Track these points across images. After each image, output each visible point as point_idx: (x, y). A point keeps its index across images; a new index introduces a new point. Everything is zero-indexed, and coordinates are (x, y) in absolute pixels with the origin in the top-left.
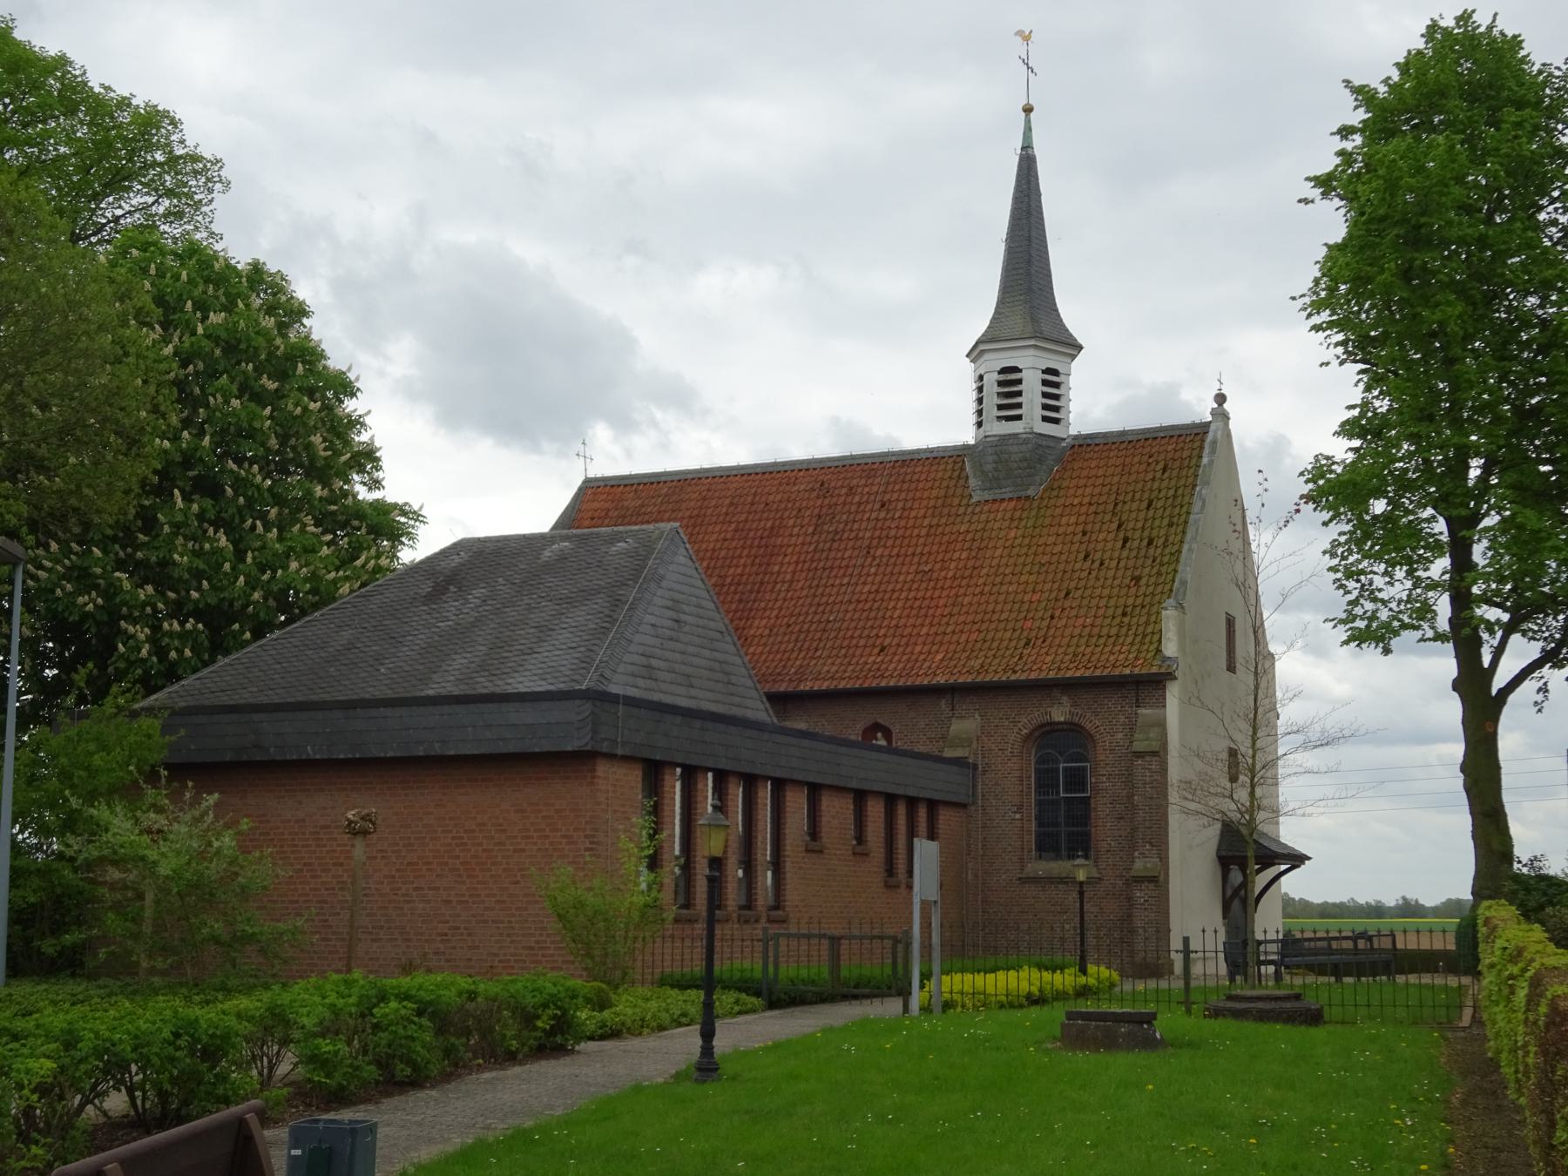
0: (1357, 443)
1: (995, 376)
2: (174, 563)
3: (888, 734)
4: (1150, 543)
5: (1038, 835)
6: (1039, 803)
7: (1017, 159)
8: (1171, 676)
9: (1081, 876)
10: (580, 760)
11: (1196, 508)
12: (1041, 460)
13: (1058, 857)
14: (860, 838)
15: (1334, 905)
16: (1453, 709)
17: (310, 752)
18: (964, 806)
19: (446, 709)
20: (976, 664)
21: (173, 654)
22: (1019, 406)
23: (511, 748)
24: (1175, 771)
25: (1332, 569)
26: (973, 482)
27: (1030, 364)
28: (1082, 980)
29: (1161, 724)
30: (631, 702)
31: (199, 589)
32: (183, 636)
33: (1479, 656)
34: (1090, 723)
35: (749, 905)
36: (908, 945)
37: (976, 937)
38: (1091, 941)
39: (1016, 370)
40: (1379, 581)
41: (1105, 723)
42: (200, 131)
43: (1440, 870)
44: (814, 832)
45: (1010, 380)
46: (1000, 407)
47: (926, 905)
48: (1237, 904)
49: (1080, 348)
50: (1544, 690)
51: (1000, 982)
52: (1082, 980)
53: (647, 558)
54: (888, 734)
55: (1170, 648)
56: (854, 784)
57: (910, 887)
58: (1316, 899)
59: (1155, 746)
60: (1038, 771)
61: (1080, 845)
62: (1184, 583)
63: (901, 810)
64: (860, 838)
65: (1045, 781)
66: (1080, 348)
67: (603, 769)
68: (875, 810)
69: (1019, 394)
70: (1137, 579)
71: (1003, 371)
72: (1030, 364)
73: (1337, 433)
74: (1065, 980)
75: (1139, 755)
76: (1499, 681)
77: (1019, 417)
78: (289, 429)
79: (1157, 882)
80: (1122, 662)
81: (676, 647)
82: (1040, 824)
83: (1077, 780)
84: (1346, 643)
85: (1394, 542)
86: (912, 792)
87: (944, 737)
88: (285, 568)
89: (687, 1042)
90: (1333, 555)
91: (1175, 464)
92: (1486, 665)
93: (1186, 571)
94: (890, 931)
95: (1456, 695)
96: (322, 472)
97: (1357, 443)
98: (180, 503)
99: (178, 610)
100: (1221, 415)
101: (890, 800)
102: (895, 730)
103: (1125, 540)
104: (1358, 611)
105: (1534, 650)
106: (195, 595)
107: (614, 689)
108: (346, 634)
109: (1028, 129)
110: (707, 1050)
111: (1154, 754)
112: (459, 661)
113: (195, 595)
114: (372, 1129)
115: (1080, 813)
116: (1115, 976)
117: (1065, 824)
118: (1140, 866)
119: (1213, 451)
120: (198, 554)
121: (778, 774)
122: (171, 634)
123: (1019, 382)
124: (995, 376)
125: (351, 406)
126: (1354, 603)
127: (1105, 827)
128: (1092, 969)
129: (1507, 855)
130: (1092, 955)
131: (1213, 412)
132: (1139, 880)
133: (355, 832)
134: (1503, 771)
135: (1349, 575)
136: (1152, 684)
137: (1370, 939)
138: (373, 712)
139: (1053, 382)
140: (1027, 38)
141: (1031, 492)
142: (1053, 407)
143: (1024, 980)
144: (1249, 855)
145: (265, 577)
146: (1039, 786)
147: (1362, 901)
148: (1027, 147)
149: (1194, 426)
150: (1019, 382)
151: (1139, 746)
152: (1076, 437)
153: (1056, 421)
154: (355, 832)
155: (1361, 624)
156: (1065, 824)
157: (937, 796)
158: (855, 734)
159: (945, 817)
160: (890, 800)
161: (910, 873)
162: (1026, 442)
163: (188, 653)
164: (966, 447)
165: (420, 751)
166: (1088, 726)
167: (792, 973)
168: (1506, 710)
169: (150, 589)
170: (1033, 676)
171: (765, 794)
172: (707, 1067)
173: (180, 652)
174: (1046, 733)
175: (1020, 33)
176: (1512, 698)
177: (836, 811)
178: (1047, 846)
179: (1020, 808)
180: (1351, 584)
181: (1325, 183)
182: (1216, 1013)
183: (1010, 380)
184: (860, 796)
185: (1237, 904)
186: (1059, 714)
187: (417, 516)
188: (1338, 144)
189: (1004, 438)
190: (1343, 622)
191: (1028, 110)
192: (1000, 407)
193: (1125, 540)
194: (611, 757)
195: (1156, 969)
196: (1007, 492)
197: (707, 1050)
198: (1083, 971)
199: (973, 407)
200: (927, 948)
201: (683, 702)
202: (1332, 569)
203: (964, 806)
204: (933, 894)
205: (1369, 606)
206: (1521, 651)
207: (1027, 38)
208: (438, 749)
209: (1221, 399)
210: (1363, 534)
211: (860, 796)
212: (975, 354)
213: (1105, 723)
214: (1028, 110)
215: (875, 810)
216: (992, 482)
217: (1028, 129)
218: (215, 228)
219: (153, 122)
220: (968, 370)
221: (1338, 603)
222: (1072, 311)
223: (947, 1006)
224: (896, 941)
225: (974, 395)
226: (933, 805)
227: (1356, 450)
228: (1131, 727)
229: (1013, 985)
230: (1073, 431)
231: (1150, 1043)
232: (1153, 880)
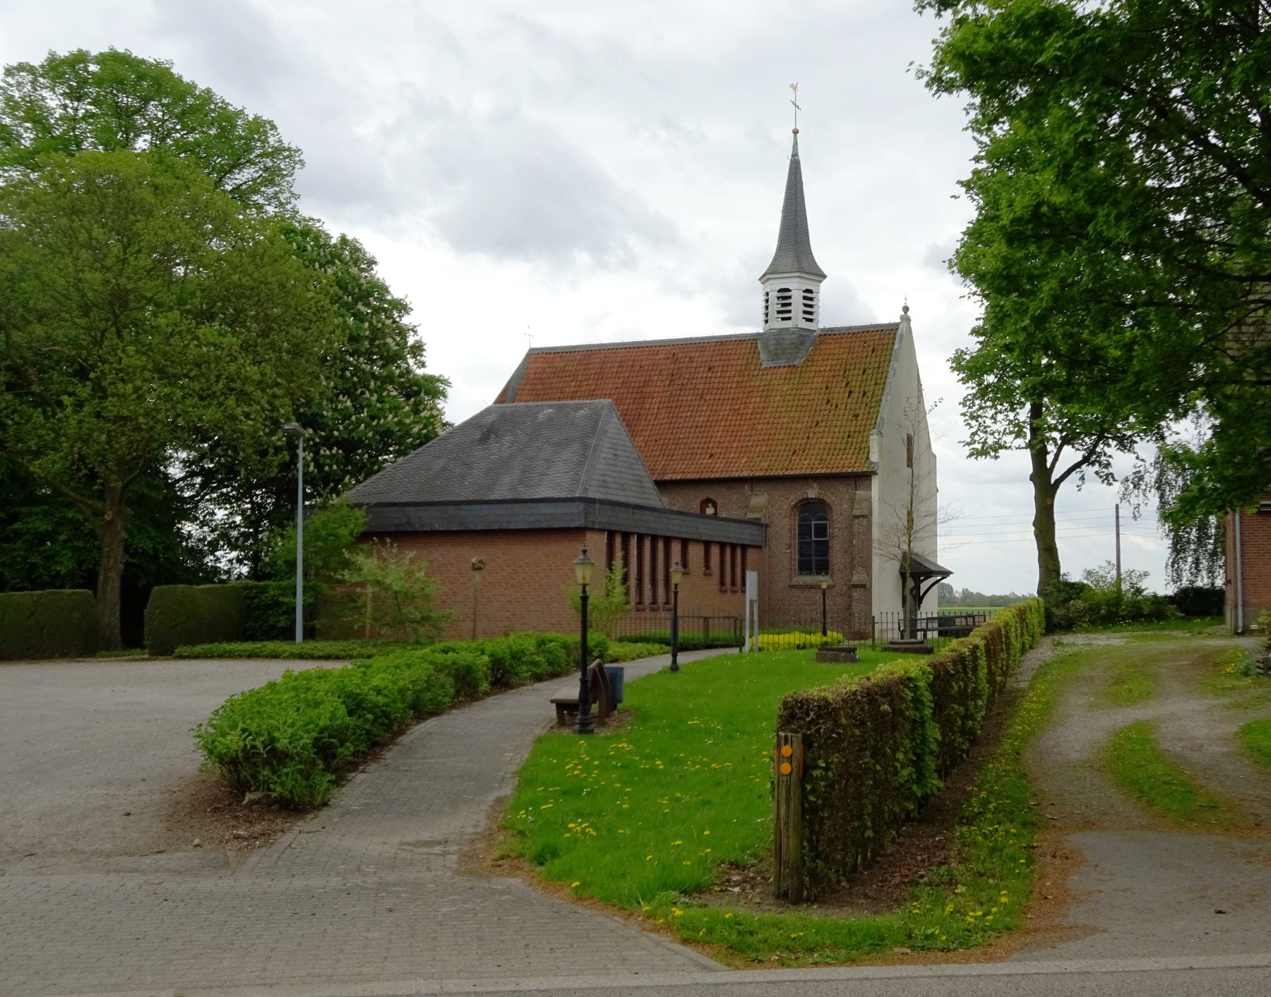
0: (982, 339)
1: (777, 294)
2: (323, 416)
3: (715, 505)
4: (865, 394)
5: (800, 562)
6: (800, 543)
7: (788, 162)
8: (875, 473)
9: (824, 586)
10: (579, 531)
11: (890, 375)
12: (802, 344)
13: (811, 574)
14: (707, 566)
15: (1000, 597)
16: (1029, 491)
17: (437, 527)
18: (759, 547)
19: (509, 506)
20: (765, 465)
21: (327, 468)
22: (790, 311)
23: (543, 525)
24: (876, 533)
25: (964, 414)
26: (762, 356)
27: (796, 286)
28: (825, 639)
29: (869, 500)
30: (602, 502)
31: (338, 430)
32: (332, 456)
33: (1045, 461)
34: (829, 498)
35: (654, 602)
36: (743, 621)
37: (771, 619)
38: (829, 620)
39: (788, 290)
40: (989, 422)
41: (837, 498)
42: (287, 134)
43: (1023, 580)
44: (685, 565)
45: (784, 295)
46: (779, 312)
47: (752, 602)
48: (914, 598)
49: (825, 277)
50: (1082, 478)
51: (784, 639)
52: (825, 639)
53: (597, 421)
54: (715, 505)
55: (874, 457)
56: (705, 538)
57: (744, 592)
58: (988, 593)
59: (865, 512)
60: (800, 526)
61: (823, 567)
62: (883, 419)
63: (728, 551)
64: (707, 566)
65: (804, 531)
66: (825, 277)
67: (589, 535)
68: (715, 551)
69: (790, 304)
70: (856, 416)
71: (781, 291)
72: (796, 286)
73: (972, 333)
74: (816, 638)
75: (857, 517)
76: (1055, 476)
77: (789, 319)
78: (376, 334)
79: (865, 587)
80: (847, 464)
81: (610, 465)
82: (801, 555)
83: (821, 531)
84: (970, 456)
85: (1003, 395)
86: (734, 541)
87: (747, 507)
88: (386, 418)
89: (667, 660)
90: (965, 406)
91: (880, 347)
92: (1048, 465)
93: (884, 412)
94: (734, 614)
95: (1031, 484)
96: (391, 358)
97: (982, 339)
98: (324, 383)
99: (328, 442)
100: (906, 319)
101: (722, 545)
102: (719, 502)
103: (850, 392)
104: (977, 438)
105: (1079, 456)
106: (336, 433)
107: (591, 495)
108: (440, 463)
109: (796, 144)
110: (674, 661)
111: (865, 516)
112: (507, 479)
113: (336, 433)
114: (622, 669)
115: (824, 548)
116: (840, 636)
117: (814, 557)
118: (856, 579)
119: (901, 341)
120: (335, 410)
121: (668, 534)
122: (325, 456)
123: (790, 297)
124: (777, 294)
125: (406, 320)
126: (974, 434)
127: (837, 557)
128: (829, 633)
129: (1057, 570)
130: (828, 626)
131: (902, 317)
132: (855, 586)
133: (476, 568)
134: (1057, 527)
135: (972, 418)
136: (863, 478)
137: (974, 617)
138: (472, 507)
139: (809, 295)
140: (794, 88)
141: (796, 363)
142: (809, 314)
143: (796, 637)
144: (918, 573)
145: (375, 423)
146: (800, 534)
147: (1019, 594)
148: (795, 155)
149: (890, 325)
150: (790, 297)
151: (857, 512)
152: (822, 330)
153: (811, 320)
154: (476, 568)
155: (979, 446)
156: (814, 557)
157: (747, 543)
158: (695, 507)
159: (751, 554)
160: (722, 545)
161: (744, 584)
162: (793, 333)
163: (335, 467)
164: (758, 334)
165: (496, 527)
166: (828, 500)
167: (686, 635)
168: (1059, 491)
169: (311, 431)
170: (797, 472)
171: (676, 548)
172: (675, 668)
173: (331, 467)
174: (805, 506)
175: (792, 86)
176: (1062, 485)
177: (696, 552)
178: (804, 567)
179: (789, 547)
180: (973, 423)
181: (967, 185)
182: (886, 649)
183: (784, 295)
184: (707, 544)
185: (914, 598)
186: (813, 492)
187: (446, 382)
188: (974, 166)
189: (780, 330)
190: (968, 444)
191: (796, 132)
192: (779, 312)
193: (850, 392)
194: (593, 529)
195: (861, 636)
196: (783, 363)
197: (674, 661)
198: (825, 634)
199: (763, 310)
200: (752, 622)
201: (622, 499)
202: (964, 414)
203: (759, 547)
204: (755, 597)
205: (982, 435)
206: (1071, 455)
207: (794, 88)
208: (505, 526)
209: (906, 309)
210: (983, 392)
211: (707, 544)
212: (764, 279)
213: (837, 498)
214: (796, 132)
215: (715, 551)
216: (774, 356)
217: (796, 144)
218: (294, 190)
219: (260, 128)
220: (760, 289)
221: (966, 434)
222: (821, 252)
223: (760, 649)
224: (736, 619)
225: (764, 304)
226: (744, 547)
227: (981, 343)
228: (852, 501)
229: (792, 640)
230: (821, 326)
231: (854, 660)
232: (863, 586)
